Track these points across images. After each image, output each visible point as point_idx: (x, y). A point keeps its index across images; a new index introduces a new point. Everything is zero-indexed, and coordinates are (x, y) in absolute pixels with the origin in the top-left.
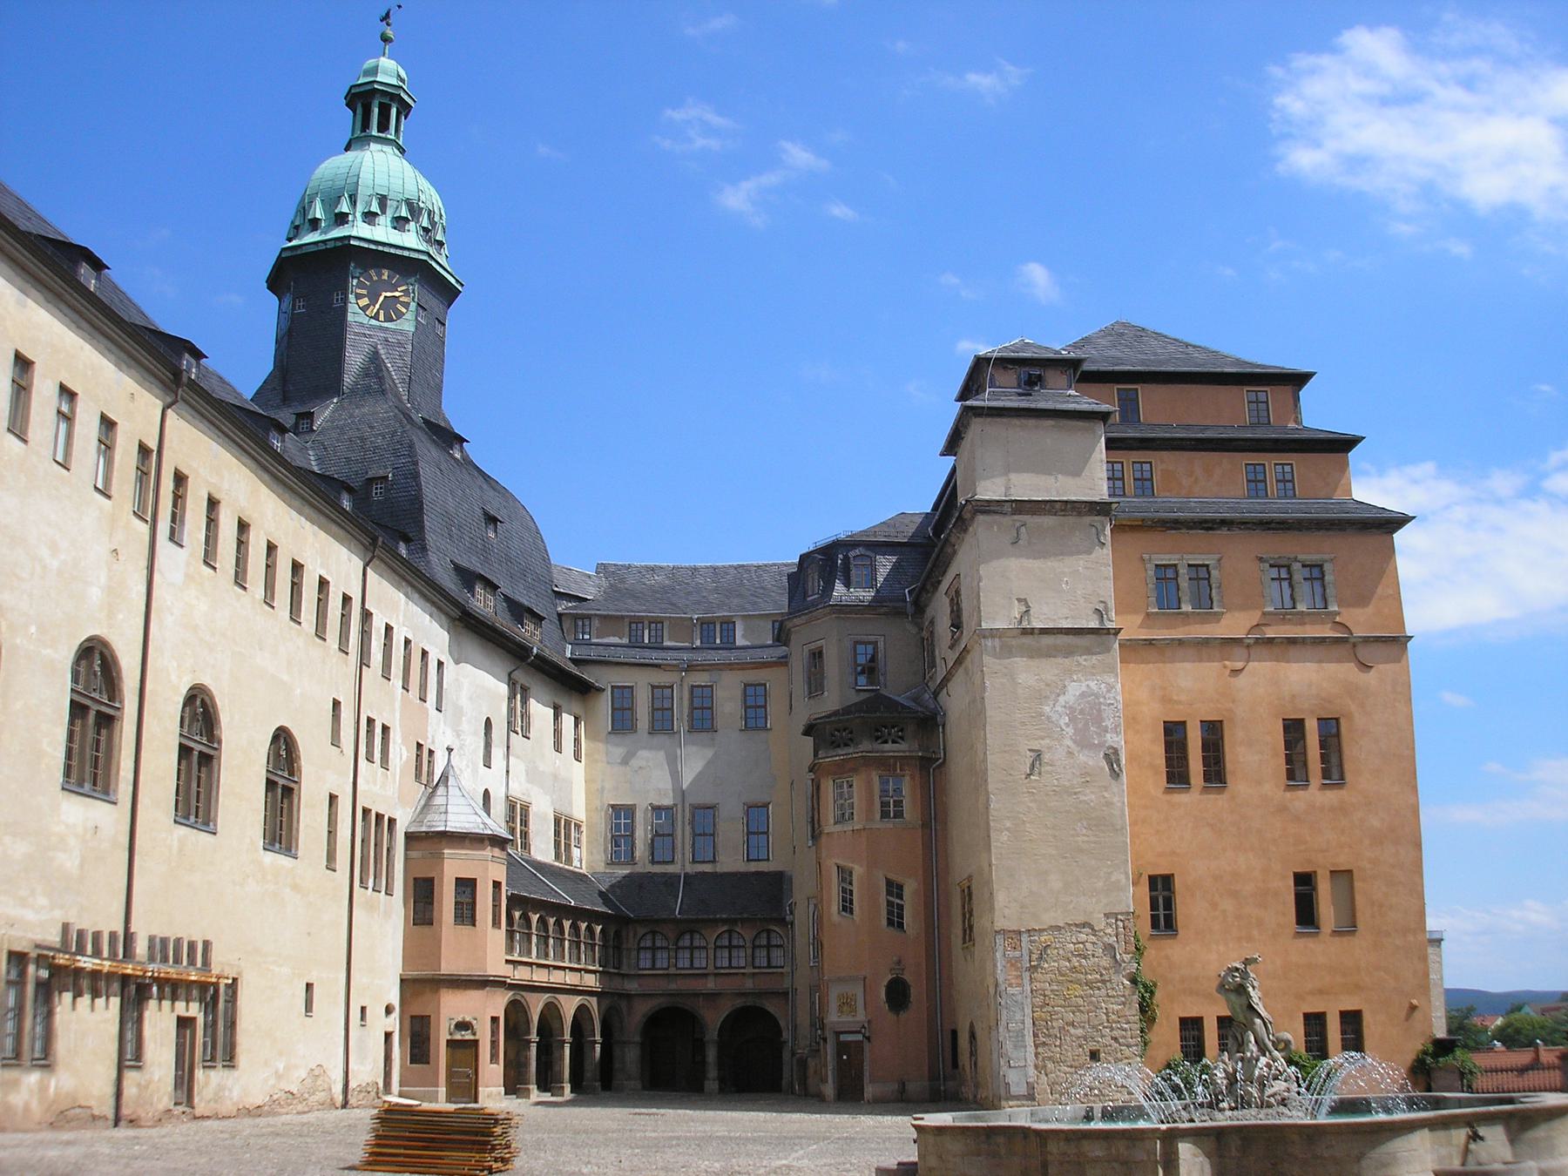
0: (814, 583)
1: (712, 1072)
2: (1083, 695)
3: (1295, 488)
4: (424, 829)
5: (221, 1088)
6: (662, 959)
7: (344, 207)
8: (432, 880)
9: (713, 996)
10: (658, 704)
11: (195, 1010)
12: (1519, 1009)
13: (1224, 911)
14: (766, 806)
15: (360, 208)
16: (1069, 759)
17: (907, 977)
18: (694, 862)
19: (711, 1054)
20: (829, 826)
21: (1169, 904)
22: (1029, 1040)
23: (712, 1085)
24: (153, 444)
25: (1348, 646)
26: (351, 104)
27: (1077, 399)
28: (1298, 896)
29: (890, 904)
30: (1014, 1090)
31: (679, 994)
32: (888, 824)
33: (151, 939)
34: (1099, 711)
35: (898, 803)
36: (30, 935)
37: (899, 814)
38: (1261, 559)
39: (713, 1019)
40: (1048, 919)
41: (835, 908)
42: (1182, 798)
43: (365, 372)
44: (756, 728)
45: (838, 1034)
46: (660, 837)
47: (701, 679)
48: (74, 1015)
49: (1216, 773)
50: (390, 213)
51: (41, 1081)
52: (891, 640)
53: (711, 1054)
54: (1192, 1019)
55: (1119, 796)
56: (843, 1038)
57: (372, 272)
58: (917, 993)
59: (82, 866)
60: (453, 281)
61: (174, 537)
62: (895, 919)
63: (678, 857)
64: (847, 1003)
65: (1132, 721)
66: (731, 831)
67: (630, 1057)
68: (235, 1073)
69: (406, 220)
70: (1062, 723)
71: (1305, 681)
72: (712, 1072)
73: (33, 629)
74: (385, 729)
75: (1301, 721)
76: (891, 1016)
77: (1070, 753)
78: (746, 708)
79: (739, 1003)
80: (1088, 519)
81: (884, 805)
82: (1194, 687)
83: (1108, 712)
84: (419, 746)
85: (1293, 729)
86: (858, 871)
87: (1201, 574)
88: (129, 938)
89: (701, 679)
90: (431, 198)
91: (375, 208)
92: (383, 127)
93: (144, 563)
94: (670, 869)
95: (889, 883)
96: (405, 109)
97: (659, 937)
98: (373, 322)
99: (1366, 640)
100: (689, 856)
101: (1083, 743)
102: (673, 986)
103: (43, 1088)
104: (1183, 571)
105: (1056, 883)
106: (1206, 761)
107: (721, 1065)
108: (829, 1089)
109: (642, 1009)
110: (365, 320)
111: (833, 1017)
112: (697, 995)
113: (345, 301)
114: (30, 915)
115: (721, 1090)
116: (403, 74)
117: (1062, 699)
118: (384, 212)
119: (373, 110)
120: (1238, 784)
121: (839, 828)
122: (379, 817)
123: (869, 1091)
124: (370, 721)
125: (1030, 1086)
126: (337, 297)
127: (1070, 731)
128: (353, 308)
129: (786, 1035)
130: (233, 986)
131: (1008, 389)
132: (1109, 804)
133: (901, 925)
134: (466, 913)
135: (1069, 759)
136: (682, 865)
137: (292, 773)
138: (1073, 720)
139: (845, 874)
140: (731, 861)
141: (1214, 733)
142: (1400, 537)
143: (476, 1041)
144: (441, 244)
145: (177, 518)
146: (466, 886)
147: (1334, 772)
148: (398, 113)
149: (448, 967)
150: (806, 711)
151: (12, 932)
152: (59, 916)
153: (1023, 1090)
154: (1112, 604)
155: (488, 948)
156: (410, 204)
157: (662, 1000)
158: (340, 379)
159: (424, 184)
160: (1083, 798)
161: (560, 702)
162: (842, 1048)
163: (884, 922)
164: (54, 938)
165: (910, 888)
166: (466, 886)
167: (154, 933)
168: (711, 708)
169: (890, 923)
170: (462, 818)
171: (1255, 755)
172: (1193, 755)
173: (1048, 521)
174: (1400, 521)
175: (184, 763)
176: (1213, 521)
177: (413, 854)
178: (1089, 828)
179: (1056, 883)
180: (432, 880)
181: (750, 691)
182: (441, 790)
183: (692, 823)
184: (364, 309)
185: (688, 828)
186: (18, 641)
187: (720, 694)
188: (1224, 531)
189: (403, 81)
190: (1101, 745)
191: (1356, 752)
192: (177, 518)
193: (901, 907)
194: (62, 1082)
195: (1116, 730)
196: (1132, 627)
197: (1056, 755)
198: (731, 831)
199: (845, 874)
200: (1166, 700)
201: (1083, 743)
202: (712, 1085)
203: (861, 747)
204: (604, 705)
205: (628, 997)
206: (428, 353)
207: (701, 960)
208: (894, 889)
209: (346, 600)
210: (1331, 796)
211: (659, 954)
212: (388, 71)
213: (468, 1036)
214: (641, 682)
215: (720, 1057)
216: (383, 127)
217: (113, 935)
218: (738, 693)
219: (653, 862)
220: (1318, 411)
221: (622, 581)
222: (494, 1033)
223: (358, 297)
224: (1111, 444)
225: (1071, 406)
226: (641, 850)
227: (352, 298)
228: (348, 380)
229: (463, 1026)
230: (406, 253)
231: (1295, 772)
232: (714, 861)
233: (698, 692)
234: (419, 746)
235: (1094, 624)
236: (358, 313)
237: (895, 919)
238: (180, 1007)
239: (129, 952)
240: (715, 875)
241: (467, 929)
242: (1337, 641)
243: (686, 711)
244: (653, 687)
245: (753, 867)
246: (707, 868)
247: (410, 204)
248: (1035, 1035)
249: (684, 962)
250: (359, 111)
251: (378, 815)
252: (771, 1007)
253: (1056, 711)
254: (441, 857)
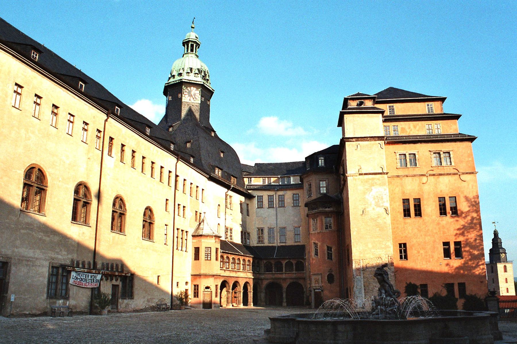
1: (285, 300)
5: (127, 305)
7: (181, 71)
9: (285, 279)
10: (270, 200)
11: (119, 283)
12: (386, 275)
13: (422, 254)
15: (185, 71)
17: (333, 273)
18: (280, 243)
20: (312, 232)
21: (405, 251)
23: (285, 304)
24: (102, 130)
26: (184, 45)
28: (444, 249)
29: (328, 253)
31: (276, 279)
32: (327, 231)
33: (103, 264)
36: (60, 262)
39: (285, 285)
42: (408, 220)
44: (297, 206)
45: (315, 289)
49: (418, 213)
50: (193, 72)
51: (64, 302)
54: (424, 285)
55: (388, 219)
56: (316, 291)
57: (189, 88)
58: (336, 277)
61: (110, 154)
62: (330, 257)
63: (275, 241)
64: (317, 281)
65: (392, 200)
67: (262, 295)
72: (285, 300)
77: (374, 209)
78: (294, 200)
79: (291, 281)
82: (411, 188)
84: (196, 212)
86: (319, 244)
88: (95, 263)
89: (281, 193)
90: (205, 68)
91: (189, 71)
92: (192, 50)
94: (274, 245)
95: (328, 247)
96: (198, 45)
102: (274, 277)
103: (64, 304)
105: (370, 246)
106: (415, 210)
107: (287, 298)
109: (265, 283)
113: (182, 96)
114: (60, 257)
115: (287, 305)
119: (190, 46)
121: (314, 232)
126: (180, 95)
129: (305, 290)
131: (354, 105)
132: (385, 223)
134: (208, 257)
136: (277, 243)
140: (290, 242)
144: (208, 80)
145: (110, 151)
146: (209, 248)
148: (196, 46)
149: (202, 272)
150: (306, 199)
155: (214, 266)
156: (198, 70)
159: (203, 64)
162: (316, 293)
164: (68, 262)
169: (328, 258)
171: (430, 208)
172: (412, 208)
176: (416, 141)
178: (380, 230)
179: (370, 246)
180: (198, 248)
181: (295, 196)
182: (202, 223)
186: (55, 182)
187: (286, 197)
192: (110, 151)
194: (71, 302)
196: (393, 172)
197: (369, 209)
201: (378, 205)
202: (285, 304)
205: (262, 279)
206: (205, 108)
212: (192, 36)
215: (287, 295)
216: (192, 50)
217: (89, 264)
218: (291, 196)
219: (269, 243)
221: (261, 168)
222: (217, 289)
227: (183, 95)
235: (381, 172)
236: (186, 98)
238: (114, 282)
240: (286, 246)
242: (454, 174)
243: (277, 202)
244: (268, 196)
245: (296, 244)
246: (284, 244)
247: (198, 70)
248: (365, 290)
250: (186, 46)
252: (301, 282)
254: (200, 241)
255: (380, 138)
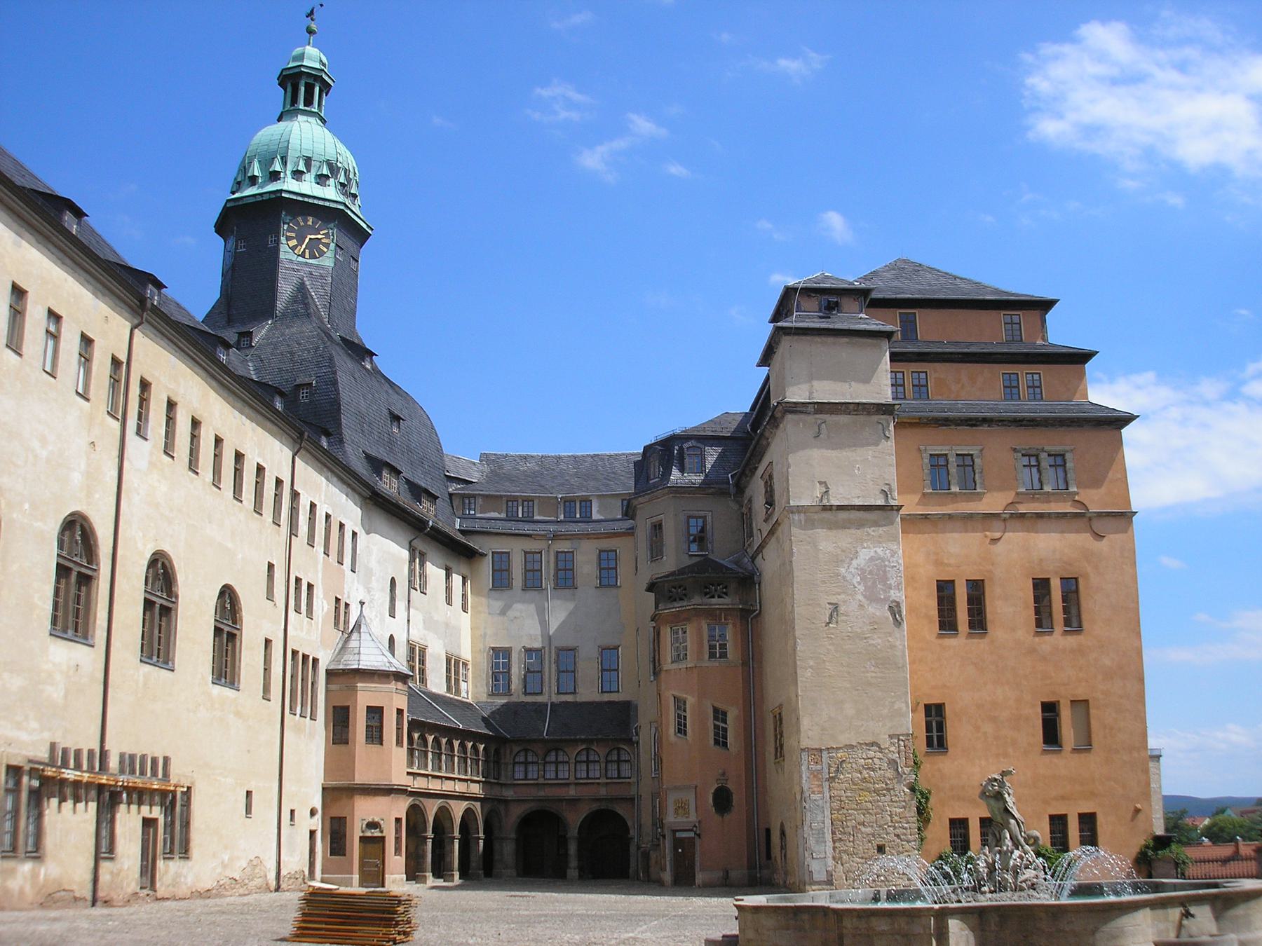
0: (655, 469)
1: (573, 863)
2: (872, 559)
3: (1042, 392)
4: (341, 667)
5: (178, 875)
6: (533, 772)
7: (277, 167)
8: (348, 708)
9: (574, 801)
10: (529, 567)
11: (157, 813)
12: (1223, 811)
13: (985, 733)
14: (616, 648)
15: (290, 168)
16: (861, 611)
17: (730, 786)
18: (559, 693)
19: (573, 848)
20: (667, 664)
21: (941, 727)
22: (829, 837)
23: (573, 872)
24: (123, 357)
25: (1085, 520)
26: (282, 84)
27: (866, 321)
28: (1045, 721)
29: (716, 727)
30: (816, 877)
31: (547, 800)
32: (715, 663)
33: (122, 756)
34: (885, 572)
35: (723, 646)
36: (24, 752)
37: (724, 655)
38: (1015, 450)
39: (574, 820)
40: (844, 739)
41: (672, 731)
42: (951, 642)
43: (294, 300)
44: (609, 586)
45: (674, 831)
46: (531, 673)
47: (564, 546)
48: (59, 817)
49: (978, 622)
50: (314, 171)
51: (33, 869)
52: (717, 515)
53: (573, 848)
54: (960, 820)
55: (901, 640)
56: (678, 835)
57: (300, 219)
58: (738, 799)
59: (66, 697)
60: (364, 226)
61: (140, 432)
62: (721, 740)
63: (546, 689)
64: (681, 807)
65: (911, 580)
66: (588, 668)
67: (507, 850)
68: (189, 863)
69: (327, 177)
70: (855, 581)
71: (1051, 548)
72: (573, 863)
73: (26, 506)
74: (310, 586)
75: (1047, 580)
76: (717, 818)
77: (861, 606)
78: (601, 569)
79: (595, 806)
80: (875, 418)
81: (712, 647)
82: (961, 553)
83: (891, 573)
84: (338, 600)
85: (1041, 587)
86: (691, 700)
87: (966, 461)
88: (104, 754)
89: (564, 546)
90: (347, 159)
91: (302, 167)
92: (308, 102)
93: (116, 453)
94: (539, 699)
95: (716, 710)
96: (326, 87)
97: (530, 754)
98: (301, 259)
99: (1100, 515)
100: (554, 688)
101: (872, 598)
102: (542, 793)
103: (34, 875)
104: (952, 459)
105: (850, 710)
106: (971, 612)
107: (580, 857)
108: (667, 876)
109: (517, 812)
110: (294, 258)
111: (671, 818)
112: (561, 800)
113: (278, 242)
114: (24, 736)
115: (581, 877)
116: (324, 60)
117: (854, 562)
118: (309, 170)
119: (300, 88)
120: (997, 631)
121: (675, 666)
122: (305, 657)
123: (700, 877)
124: (298, 580)
125: (829, 874)
126: (271, 239)
127: (861, 588)
128: (284, 247)
129: (633, 833)
130: (188, 793)
131: (811, 313)
132: (893, 647)
133: (725, 744)
134: (375, 735)
135: (861, 611)
136: (549, 696)
137: (235, 622)
138: (863, 579)
139: (680, 703)
140: (588, 692)
141: (977, 590)
142: (1126, 432)
143: (383, 838)
144: (355, 196)
145: (142, 417)
146: (375, 713)
147: (1073, 621)
148: (321, 91)
149: (361, 778)
150: (649, 572)
151: (10, 750)
152: (48, 737)
153: (823, 877)
154: (895, 486)
155: (393, 763)
156: (330, 164)
157: (532, 804)
158: (273, 305)
159: (342, 148)
160: (871, 642)
161: (450, 564)
162: (678, 843)
163: (712, 742)
164: (43, 754)
165: (733, 714)
166: (375, 713)
167: (124, 750)
168: (572, 570)
169: (716, 742)
170: (372, 658)
171: (1010, 608)
172: (960, 607)
173: (843, 419)
174: (1127, 419)
175: (148, 613)
176: (976, 419)
177: (333, 687)
178: (876, 666)
179: (850, 710)
180: (348, 708)
181: (604, 556)
182: (355, 636)
183: (557, 662)
184: (293, 248)
185: (554, 666)
186: (15, 516)
187: (579, 558)
188: (985, 427)
189: (324, 65)
190: (886, 599)
191: (1092, 605)
192: (142, 417)
193: (725, 730)
194: (50, 870)
195: (898, 588)
196: (911, 504)
197: (850, 607)
198: (588, 668)
199: (680, 703)
200: (938, 563)
201: (872, 598)
202: (573, 872)
203: (693, 601)
204: (486, 567)
205: (506, 802)
206: (345, 284)
207: (564, 772)
208: (720, 715)
209: (279, 482)
210: (1072, 641)
211: (530, 768)
212: (313, 57)
213: (377, 833)
214: (516, 548)
215: (579, 850)
216: (308, 102)
217: (91, 752)
218: (594, 557)
219: (526, 693)
220: (1061, 331)
221: (501, 467)
222: (398, 831)
223: (288, 239)
224: (894, 357)
225: (862, 327)
226: (516, 683)
227: (283, 239)
228: (280, 305)
229: (373, 825)
230: (327, 204)
231: (1042, 621)
232: (574, 693)
233: (562, 556)
234: (338, 600)
235: (881, 502)
236: (288, 252)
237: (721, 740)
238: (145, 810)
239: (103, 766)
240: (575, 704)
241: (376, 748)
242: (1076, 515)
243: (552, 572)
244: (526, 553)
245: (606, 698)
246: (569, 698)
247: (330, 164)
248: (833, 833)
249: (550, 774)
250: (289, 89)
251: (304, 656)
252: (621, 810)
253: (850, 572)
254: (355, 689)
255: (884, 409)
